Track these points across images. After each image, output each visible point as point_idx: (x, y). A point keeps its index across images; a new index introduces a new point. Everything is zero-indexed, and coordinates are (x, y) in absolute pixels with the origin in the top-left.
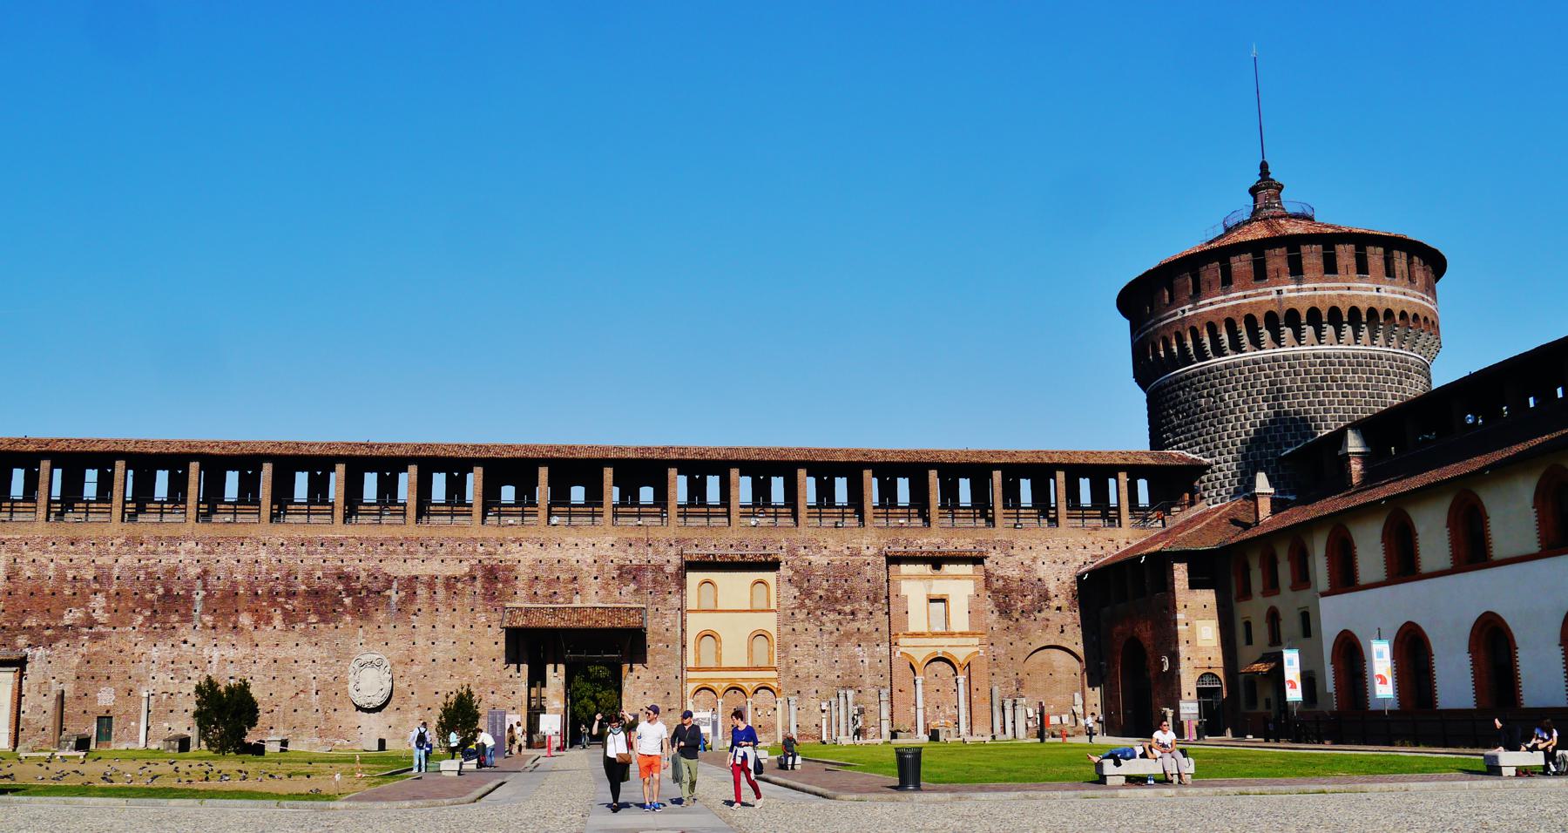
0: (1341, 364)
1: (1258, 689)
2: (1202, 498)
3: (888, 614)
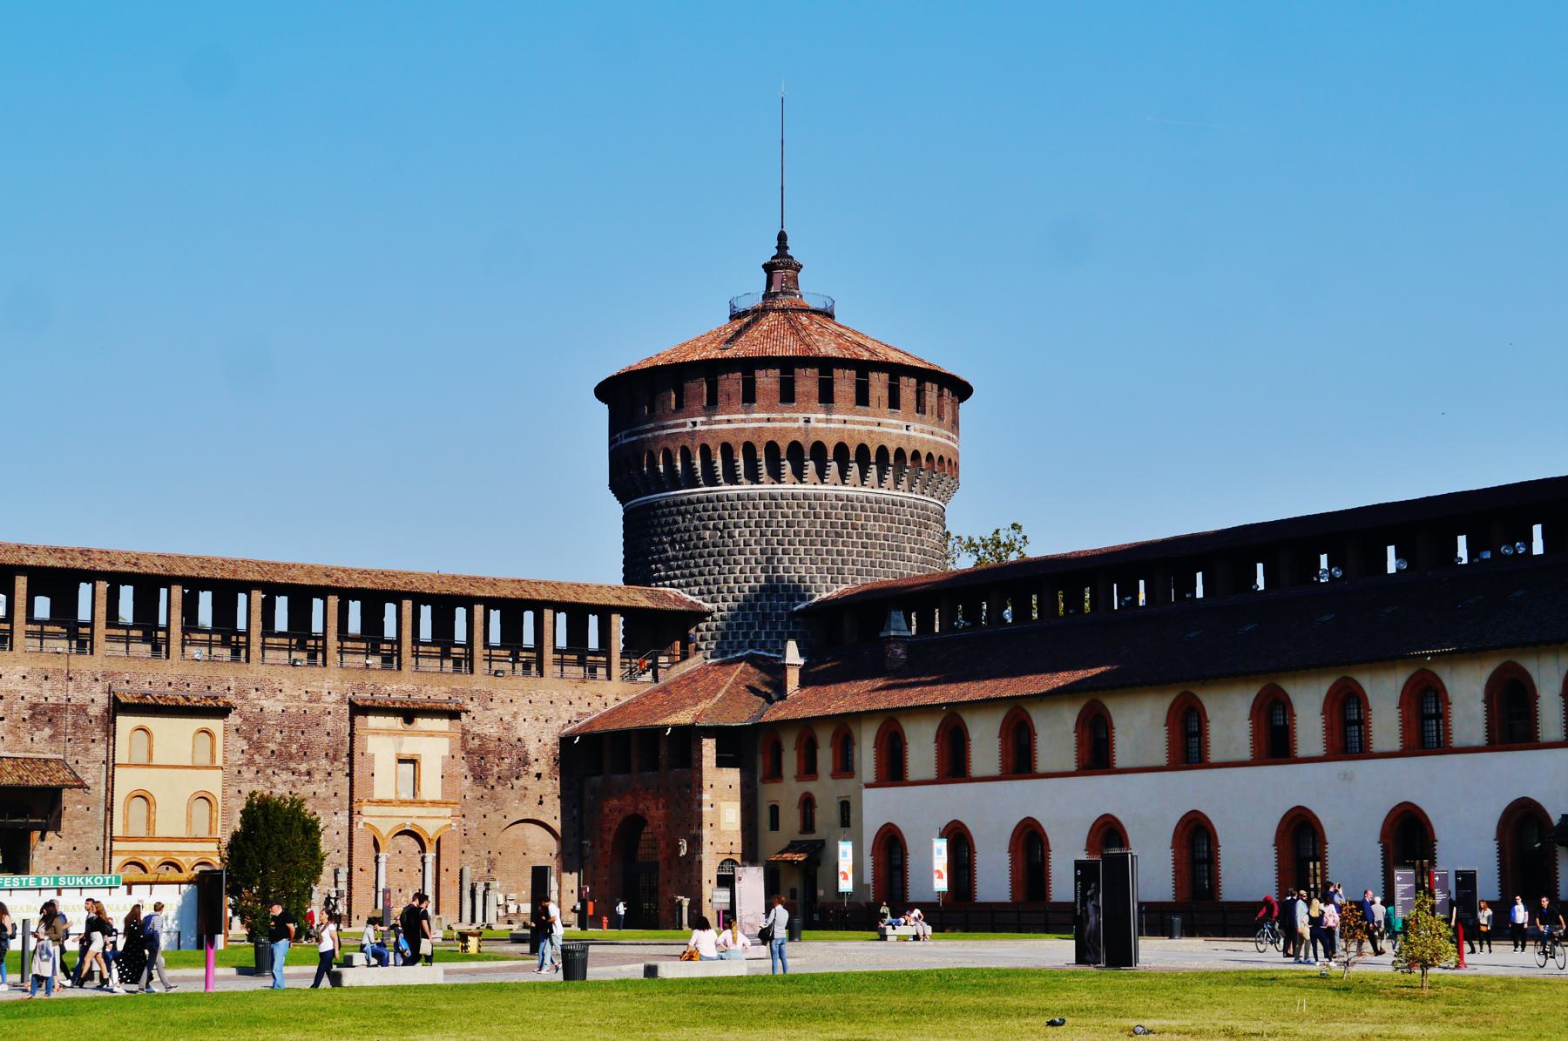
0: (863, 509)
1: (782, 877)
2: (698, 649)
3: (351, 775)
